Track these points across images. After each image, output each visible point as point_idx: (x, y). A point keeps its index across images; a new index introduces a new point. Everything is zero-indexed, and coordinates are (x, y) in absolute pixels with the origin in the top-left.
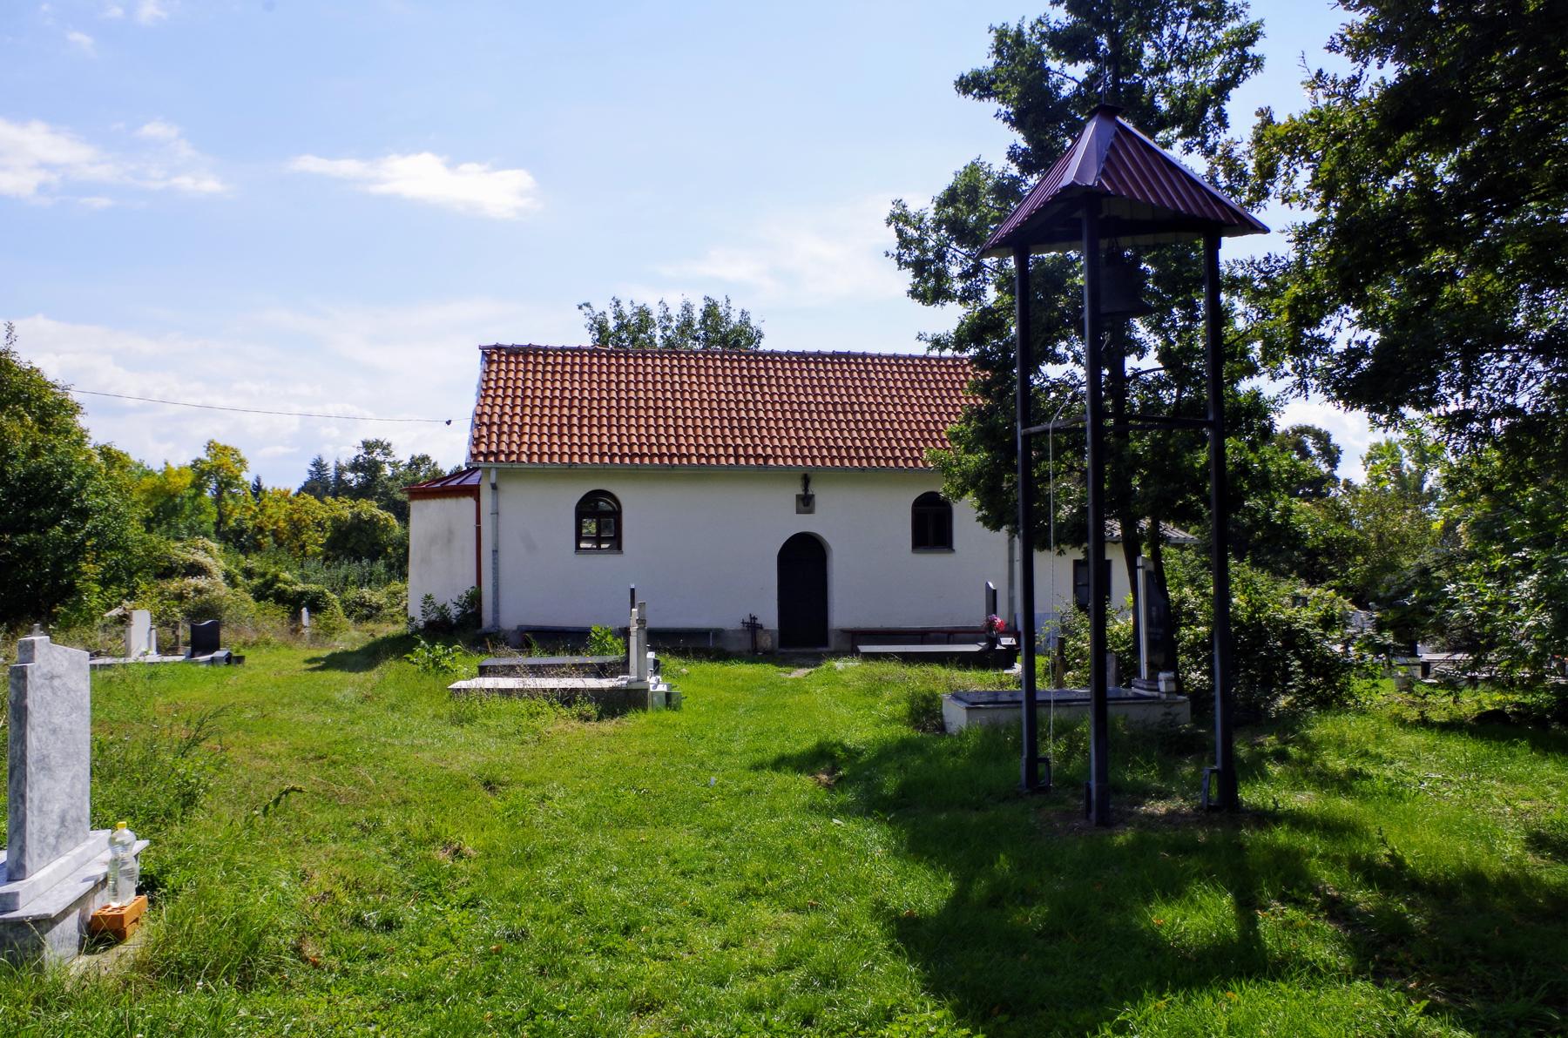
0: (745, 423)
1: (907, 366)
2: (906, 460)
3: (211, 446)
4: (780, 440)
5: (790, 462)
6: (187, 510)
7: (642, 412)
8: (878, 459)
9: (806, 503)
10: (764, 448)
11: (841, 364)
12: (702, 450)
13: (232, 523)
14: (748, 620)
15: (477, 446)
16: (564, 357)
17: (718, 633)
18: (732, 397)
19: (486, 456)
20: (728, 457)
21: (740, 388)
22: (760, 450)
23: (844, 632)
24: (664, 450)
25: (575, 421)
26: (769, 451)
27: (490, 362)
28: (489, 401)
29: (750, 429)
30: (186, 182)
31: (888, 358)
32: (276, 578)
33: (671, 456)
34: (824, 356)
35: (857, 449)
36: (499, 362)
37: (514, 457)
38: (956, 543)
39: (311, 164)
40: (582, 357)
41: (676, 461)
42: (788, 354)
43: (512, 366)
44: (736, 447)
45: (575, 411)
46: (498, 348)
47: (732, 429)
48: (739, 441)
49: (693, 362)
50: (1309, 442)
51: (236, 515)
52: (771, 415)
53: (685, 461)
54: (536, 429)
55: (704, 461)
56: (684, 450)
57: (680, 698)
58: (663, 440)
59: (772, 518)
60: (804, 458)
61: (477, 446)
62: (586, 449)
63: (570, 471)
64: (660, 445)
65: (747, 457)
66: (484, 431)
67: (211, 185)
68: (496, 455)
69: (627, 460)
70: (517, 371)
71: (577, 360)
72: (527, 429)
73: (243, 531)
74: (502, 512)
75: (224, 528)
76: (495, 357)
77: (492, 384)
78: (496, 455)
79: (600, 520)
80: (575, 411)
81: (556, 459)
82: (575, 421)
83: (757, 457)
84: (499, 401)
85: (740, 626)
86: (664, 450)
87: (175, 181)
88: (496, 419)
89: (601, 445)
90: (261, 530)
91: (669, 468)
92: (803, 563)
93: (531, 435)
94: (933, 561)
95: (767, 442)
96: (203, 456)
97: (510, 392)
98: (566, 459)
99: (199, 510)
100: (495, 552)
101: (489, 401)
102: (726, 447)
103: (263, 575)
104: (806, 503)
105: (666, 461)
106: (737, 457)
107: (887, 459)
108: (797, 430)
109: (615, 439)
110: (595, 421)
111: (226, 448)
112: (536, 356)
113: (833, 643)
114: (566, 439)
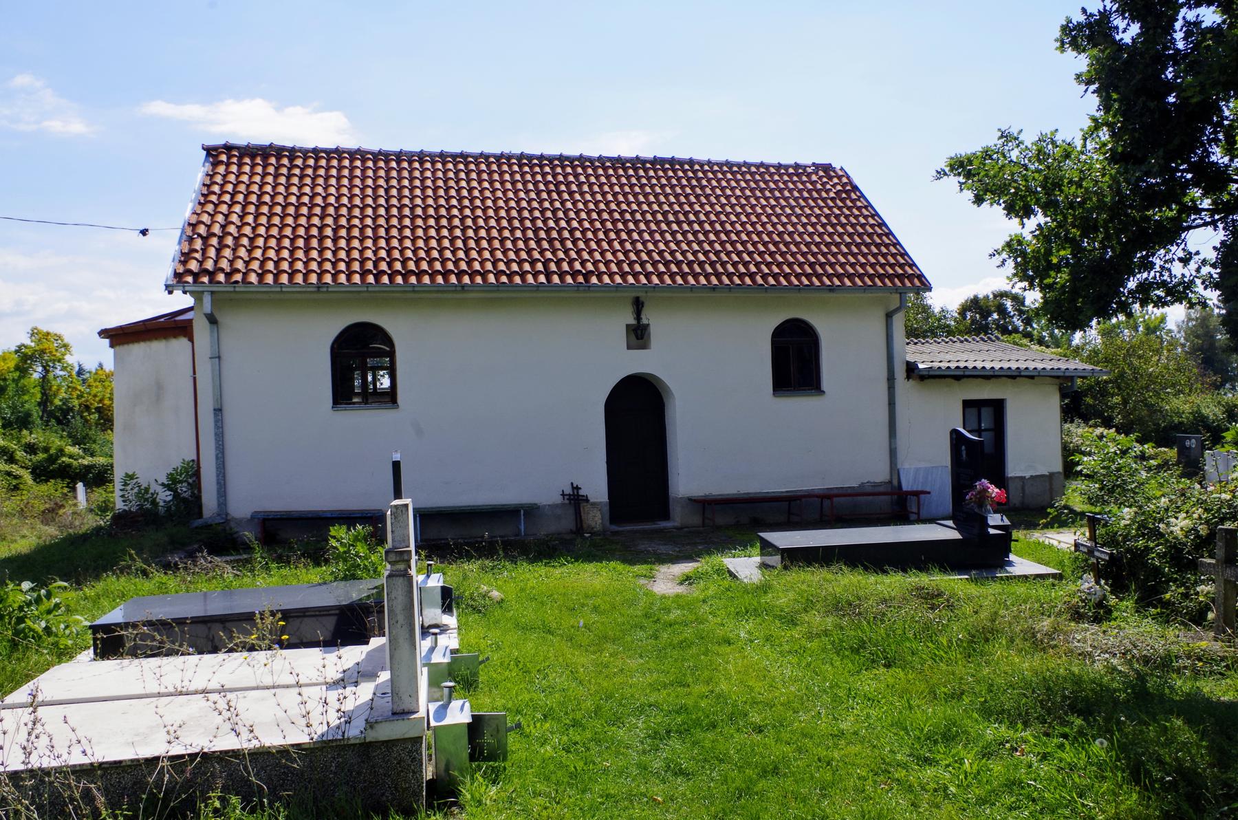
0: (554, 234)
1: (743, 174)
2: (764, 277)
3: (34, 333)
4: (602, 254)
5: (618, 279)
6: (11, 390)
7: (419, 222)
8: (730, 276)
9: (638, 335)
10: (583, 263)
11: (665, 171)
12: (502, 266)
13: (57, 402)
14: (568, 491)
15: (184, 263)
16: (317, 160)
17: (530, 511)
18: (535, 204)
19: (196, 276)
20: (536, 275)
21: (544, 195)
22: (577, 266)
23: (693, 501)
24: (450, 266)
25: (328, 232)
26: (590, 267)
27: (216, 164)
28: (210, 208)
29: (562, 241)
30: (55, 125)
31: (720, 165)
32: (61, 452)
33: (460, 274)
34: (644, 162)
35: (701, 264)
36: (228, 164)
37: (238, 277)
38: (826, 383)
39: (160, 108)
40: (340, 160)
41: (466, 279)
42: (600, 158)
43: (247, 169)
44: (546, 263)
45: (329, 221)
46: (228, 148)
47: (539, 241)
48: (549, 255)
49: (483, 167)
50: (1009, 304)
51: (62, 395)
52: (587, 225)
53: (479, 280)
54: (273, 243)
55: (504, 279)
56: (477, 266)
57: (500, 728)
58: (448, 254)
59: (593, 356)
60: (636, 275)
61: (184, 263)
62: (342, 266)
63: (319, 296)
64: (444, 262)
65: (562, 275)
66: (198, 244)
67: (77, 127)
68: (212, 275)
69: (399, 279)
70: (253, 174)
71: (335, 163)
72: (260, 242)
73: (71, 409)
74: (224, 357)
75: (50, 408)
76: (224, 158)
77: (216, 189)
78: (212, 275)
79: (359, 362)
80: (329, 221)
81: (299, 279)
82: (328, 232)
83: (574, 274)
84: (224, 208)
85: (558, 499)
86: (450, 266)
87: (46, 124)
88: (216, 229)
89: (363, 261)
90: (87, 408)
91: (455, 290)
92: (637, 413)
93: (266, 249)
94: (798, 405)
95: (586, 256)
96: (27, 342)
97: (240, 198)
98: (313, 278)
99: (23, 391)
100: (218, 411)
101: (210, 208)
102: (533, 263)
103: (46, 450)
104: (638, 335)
105: (453, 279)
106: (548, 275)
107: (741, 276)
108: (622, 243)
109: (383, 254)
110: (356, 232)
111: (48, 334)
112: (279, 158)
113: (678, 517)
114: (314, 254)
